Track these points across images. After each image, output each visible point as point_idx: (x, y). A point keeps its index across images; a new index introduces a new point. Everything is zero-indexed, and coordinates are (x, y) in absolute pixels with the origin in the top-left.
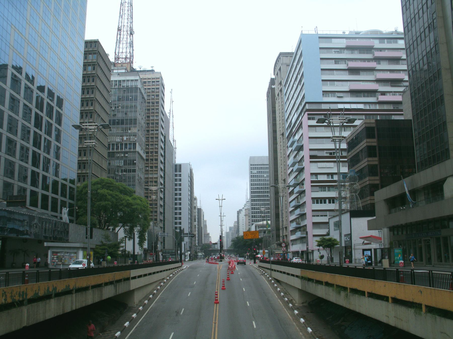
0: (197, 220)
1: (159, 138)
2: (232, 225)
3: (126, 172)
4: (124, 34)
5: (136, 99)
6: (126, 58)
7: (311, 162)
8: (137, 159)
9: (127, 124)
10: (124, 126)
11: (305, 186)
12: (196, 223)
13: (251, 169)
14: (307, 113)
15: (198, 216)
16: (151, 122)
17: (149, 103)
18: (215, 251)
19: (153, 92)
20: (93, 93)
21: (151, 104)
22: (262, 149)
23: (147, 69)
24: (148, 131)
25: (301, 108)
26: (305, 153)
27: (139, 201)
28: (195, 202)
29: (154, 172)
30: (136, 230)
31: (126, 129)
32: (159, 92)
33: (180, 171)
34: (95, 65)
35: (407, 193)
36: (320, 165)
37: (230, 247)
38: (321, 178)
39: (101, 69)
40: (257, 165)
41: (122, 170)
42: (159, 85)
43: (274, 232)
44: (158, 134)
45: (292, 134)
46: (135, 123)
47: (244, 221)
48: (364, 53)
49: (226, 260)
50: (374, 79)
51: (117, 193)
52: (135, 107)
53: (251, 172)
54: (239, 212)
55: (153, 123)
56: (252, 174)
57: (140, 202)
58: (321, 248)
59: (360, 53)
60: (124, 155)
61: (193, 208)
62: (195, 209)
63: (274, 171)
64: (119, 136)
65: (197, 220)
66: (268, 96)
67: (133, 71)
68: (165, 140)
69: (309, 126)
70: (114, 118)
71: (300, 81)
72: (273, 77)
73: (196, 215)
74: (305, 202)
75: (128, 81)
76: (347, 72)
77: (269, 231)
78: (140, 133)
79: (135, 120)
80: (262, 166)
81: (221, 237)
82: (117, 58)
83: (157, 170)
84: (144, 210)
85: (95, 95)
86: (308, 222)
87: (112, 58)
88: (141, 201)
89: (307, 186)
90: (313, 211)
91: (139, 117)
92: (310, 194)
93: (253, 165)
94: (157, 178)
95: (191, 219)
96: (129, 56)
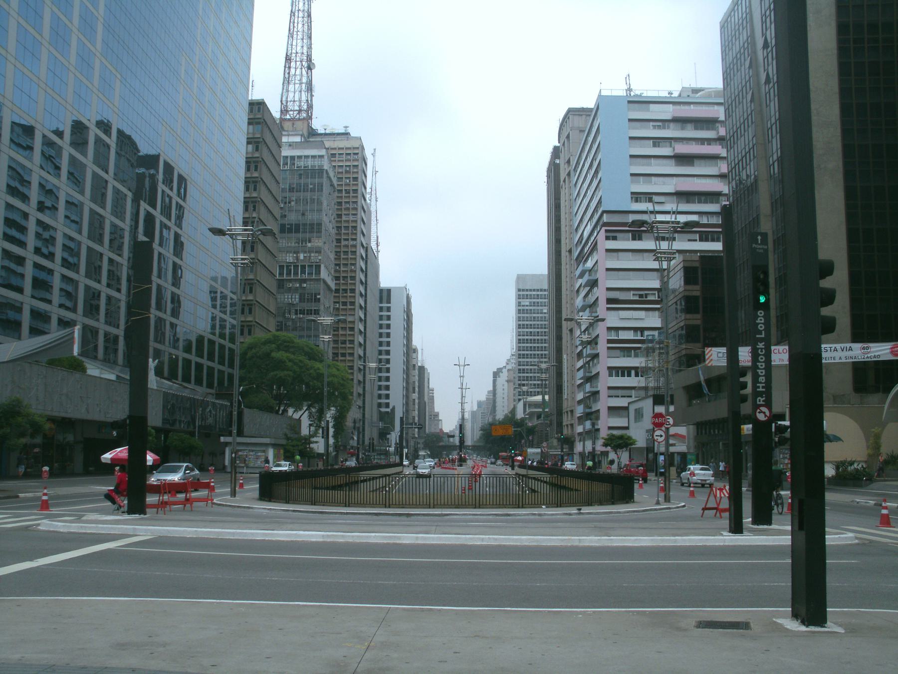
0: (417, 389)
1: (358, 253)
2: (483, 398)
3: (304, 314)
4: (297, 70)
5: (321, 190)
6: (300, 111)
7: (608, 309)
8: (322, 292)
9: (305, 232)
10: (300, 235)
11: (599, 346)
12: (415, 396)
13: (519, 297)
14: (604, 229)
15: (419, 381)
16: (344, 224)
17: (340, 191)
18: (452, 448)
19: (347, 172)
20: (255, 189)
21: (344, 194)
22: (538, 263)
23: (336, 132)
24: (339, 241)
25: (596, 217)
26: (600, 293)
27: (334, 370)
28: (414, 355)
29: (349, 313)
30: (330, 414)
31: (304, 241)
32: (357, 172)
33: (389, 301)
34: (258, 142)
35: (703, 384)
36: (623, 314)
37: (478, 441)
38: (623, 335)
39: (268, 147)
40: (531, 290)
41: (296, 310)
42: (357, 160)
43: (554, 418)
44: (355, 246)
45: (582, 258)
46: (319, 231)
47: (506, 391)
48: (702, 129)
49: (470, 463)
50: (717, 173)
51: (301, 358)
52: (320, 203)
53: (520, 303)
54: (496, 374)
55: (347, 228)
56: (521, 308)
57: (336, 373)
58: (609, 448)
59: (696, 128)
60: (301, 285)
61: (411, 368)
62: (414, 369)
63: (557, 311)
64: (291, 252)
65: (417, 389)
66: (548, 177)
67: (312, 133)
68: (366, 255)
69: (608, 251)
70: (283, 222)
71: (596, 172)
72: (558, 144)
73: (417, 379)
74: (598, 373)
75: (307, 157)
76: (673, 161)
77: (547, 415)
78: (326, 247)
79: (320, 225)
80: (539, 293)
81: (461, 427)
82: (285, 111)
83: (354, 309)
84: (343, 385)
85: (259, 194)
86: (603, 404)
87: (276, 114)
88: (338, 370)
89: (602, 347)
90: (609, 388)
91: (325, 219)
92: (607, 361)
93: (523, 290)
94: (353, 322)
95: (407, 389)
96: (305, 107)
